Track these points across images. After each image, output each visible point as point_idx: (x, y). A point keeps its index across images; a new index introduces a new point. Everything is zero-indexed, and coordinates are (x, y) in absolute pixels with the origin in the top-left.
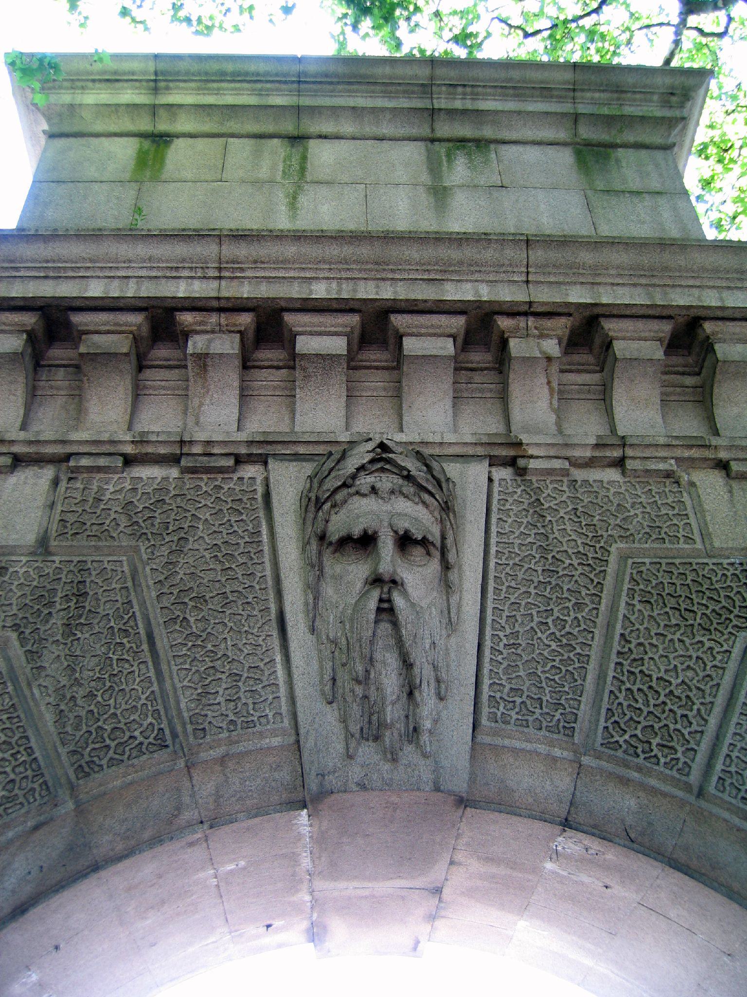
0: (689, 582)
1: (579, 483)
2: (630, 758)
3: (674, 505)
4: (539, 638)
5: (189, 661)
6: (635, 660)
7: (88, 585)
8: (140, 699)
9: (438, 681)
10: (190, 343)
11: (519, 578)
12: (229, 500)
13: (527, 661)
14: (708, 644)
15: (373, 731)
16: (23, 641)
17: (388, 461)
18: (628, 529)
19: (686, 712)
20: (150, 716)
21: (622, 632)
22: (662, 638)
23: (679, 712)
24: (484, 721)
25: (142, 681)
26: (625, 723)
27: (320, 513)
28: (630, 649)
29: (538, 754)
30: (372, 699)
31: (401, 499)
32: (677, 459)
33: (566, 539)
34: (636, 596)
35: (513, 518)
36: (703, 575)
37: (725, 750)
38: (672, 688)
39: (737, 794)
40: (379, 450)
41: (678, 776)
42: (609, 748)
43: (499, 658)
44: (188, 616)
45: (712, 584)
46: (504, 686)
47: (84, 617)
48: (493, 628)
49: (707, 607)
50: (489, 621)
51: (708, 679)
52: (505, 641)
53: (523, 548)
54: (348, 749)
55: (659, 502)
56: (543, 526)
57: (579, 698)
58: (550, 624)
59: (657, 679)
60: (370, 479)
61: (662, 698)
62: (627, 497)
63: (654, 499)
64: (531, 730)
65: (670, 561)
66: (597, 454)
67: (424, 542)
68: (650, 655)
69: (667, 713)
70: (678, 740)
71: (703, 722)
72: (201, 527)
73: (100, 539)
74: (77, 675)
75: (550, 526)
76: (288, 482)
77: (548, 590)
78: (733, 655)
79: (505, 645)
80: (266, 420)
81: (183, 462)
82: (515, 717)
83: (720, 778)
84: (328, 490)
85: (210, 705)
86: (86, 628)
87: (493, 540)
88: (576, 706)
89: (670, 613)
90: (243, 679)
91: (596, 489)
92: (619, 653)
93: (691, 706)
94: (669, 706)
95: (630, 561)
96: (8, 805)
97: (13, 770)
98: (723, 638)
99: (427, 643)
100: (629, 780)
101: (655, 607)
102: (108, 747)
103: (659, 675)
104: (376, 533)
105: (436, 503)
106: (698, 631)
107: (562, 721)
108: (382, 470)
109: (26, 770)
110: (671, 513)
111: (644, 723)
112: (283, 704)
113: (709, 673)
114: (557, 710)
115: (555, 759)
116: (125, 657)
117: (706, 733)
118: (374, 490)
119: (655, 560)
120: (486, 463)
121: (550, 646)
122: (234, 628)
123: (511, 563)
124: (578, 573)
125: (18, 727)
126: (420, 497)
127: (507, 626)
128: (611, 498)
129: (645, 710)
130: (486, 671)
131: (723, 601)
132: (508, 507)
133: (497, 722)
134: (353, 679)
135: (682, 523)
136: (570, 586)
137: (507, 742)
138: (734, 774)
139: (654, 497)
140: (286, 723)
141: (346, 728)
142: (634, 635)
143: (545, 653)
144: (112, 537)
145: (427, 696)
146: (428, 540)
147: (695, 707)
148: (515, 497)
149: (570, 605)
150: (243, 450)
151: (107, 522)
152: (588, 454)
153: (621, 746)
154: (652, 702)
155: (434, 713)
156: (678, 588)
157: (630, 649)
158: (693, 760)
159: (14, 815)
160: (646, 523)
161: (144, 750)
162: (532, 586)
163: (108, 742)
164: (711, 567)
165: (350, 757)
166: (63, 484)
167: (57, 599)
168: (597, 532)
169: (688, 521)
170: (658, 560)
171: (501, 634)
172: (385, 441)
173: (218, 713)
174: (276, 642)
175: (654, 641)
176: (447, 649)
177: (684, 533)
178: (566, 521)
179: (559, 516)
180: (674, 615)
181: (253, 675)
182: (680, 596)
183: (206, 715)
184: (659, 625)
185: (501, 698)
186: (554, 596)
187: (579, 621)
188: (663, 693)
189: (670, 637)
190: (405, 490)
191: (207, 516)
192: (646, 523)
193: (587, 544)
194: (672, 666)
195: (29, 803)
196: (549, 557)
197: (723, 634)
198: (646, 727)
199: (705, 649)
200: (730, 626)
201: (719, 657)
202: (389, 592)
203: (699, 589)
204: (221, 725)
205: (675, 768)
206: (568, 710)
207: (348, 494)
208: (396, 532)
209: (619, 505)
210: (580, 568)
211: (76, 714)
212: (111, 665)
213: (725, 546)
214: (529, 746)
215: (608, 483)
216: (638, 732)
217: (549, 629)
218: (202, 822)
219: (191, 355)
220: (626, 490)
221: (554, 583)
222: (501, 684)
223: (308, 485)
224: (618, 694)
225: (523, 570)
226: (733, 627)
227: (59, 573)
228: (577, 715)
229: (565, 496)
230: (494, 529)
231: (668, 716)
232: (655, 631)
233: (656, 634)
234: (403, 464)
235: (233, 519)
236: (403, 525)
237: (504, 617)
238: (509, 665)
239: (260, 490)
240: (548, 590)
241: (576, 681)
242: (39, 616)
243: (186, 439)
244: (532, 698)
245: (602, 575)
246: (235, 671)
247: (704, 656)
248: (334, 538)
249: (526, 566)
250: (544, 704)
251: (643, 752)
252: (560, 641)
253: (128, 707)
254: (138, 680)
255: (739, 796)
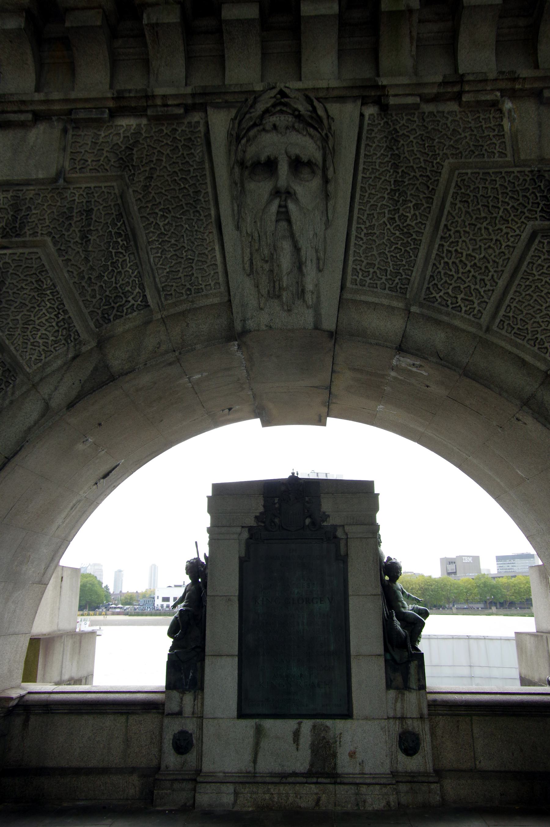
0: (497, 186)
1: (427, 114)
2: (442, 308)
3: (495, 128)
4: (388, 229)
5: (160, 251)
6: (452, 242)
7: (93, 203)
8: (131, 277)
9: (318, 259)
10: (145, 16)
11: (378, 187)
12: (182, 139)
13: (379, 244)
14: (505, 231)
15: (275, 293)
16: (55, 243)
17: (286, 105)
18: (458, 149)
19: (483, 277)
20: (137, 287)
21: (446, 223)
22: (473, 227)
23: (479, 277)
24: (348, 284)
25: (132, 265)
26: (441, 285)
27: (240, 147)
28: (450, 235)
29: (382, 305)
30: (275, 272)
31: (294, 133)
32: (501, 90)
33: (412, 158)
34: (458, 197)
35: (377, 143)
36: (509, 181)
37: (507, 302)
38: (476, 261)
39: (511, 331)
40: (279, 96)
41: (473, 319)
42: (429, 301)
43: (361, 243)
44: (158, 222)
45: (514, 187)
46: (363, 262)
47: (92, 225)
48: (358, 223)
49: (508, 204)
50: (355, 218)
51: (502, 254)
52: (365, 231)
53: (382, 165)
54: (260, 304)
55: (484, 126)
56: (397, 149)
57: (412, 269)
58: (397, 219)
59: (467, 255)
60: (274, 119)
61: (468, 268)
62: (461, 124)
63: (480, 124)
64: (379, 290)
65: (486, 171)
66: (441, 90)
67: (310, 164)
68: (463, 238)
69: (470, 278)
70: (476, 295)
71: (495, 284)
72: (164, 159)
73: (98, 171)
74: (91, 263)
75: (402, 148)
76: (220, 123)
77: (397, 195)
78: (522, 237)
79: (365, 234)
80: (204, 78)
81: (149, 112)
82: (368, 281)
83: (501, 320)
84: (244, 129)
85: (174, 279)
86: (94, 233)
87: (361, 160)
88: (410, 274)
89: (481, 209)
90: (195, 261)
91: (438, 118)
92: (442, 238)
93: (488, 273)
94: (473, 273)
95: (457, 172)
96: (55, 346)
97: (57, 325)
98: (517, 226)
99: (311, 233)
100: (440, 321)
101: (471, 205)
102: (113, 307)
103: (468, 253)
104: (276, 158)
105: (318, 135)
106: (499, 221)
107: (400, 284)
108: (282, 112)
109: (65, 324)
110: (491, 134)
111: (454, 285)
112: (220, 277)
113: (504, 250)
114: (396, 277)
115: (393, 308)
116: (120, 250)
117: (495, 292)
118: (275, 127)
119: (475, 171)
120: (359, 103)
121: (395, 234)
122: (188, 228)
123: (373, 176)
124: (419, 182)
125: (57, 298)
126: (307, 131)
127: (367, 221)
128: (449, 125)
129: (456, 276)
130: (351, 252)
131: (521, 199)
132: (373, 135)
133: (356, 285)
134: (262, 260)
135: (499, 142)
136: (412, 192)
137: (363, 298)
138: (511, 318)
139: (481, 122)
140: (223, 288)
141: (259, 292)
142: (454, 225)
143: (392, 239)
144: (107, 170)
145: (310, 270)
146: (312, 162)
147: (490, 274)
148: (379, 127)
149: (411, 205)
150: (190, 101)
151: (102, 159)
152: (435, 91)
153: (437, 300)
154: (461, 270)
155: (315, 280)
156: (489, 190)
157: (450, 235)
158: (485, 309)
159: (60, 351)
160: (472, 143)
161: (135, 309)
162: (386, 192)
163: (113, 304)
164: (516, 174)
165: (262, 309)
166: (70, 132)
167: (74, 214)
168: (435, 151)
169: (504, 140)
170: (478, 170)
171: (363, 227)
172: (284, 89)
173: (180, 284)
174: (215, 236)
175: (467, 229)
176: (325, 238)
177: (499, 150)
178: (414, 144)
179: (409, 140)
180: (484, 210)
181: (201, 259)
182: (490, 197)
183: (172, 286)
184: (472, 217)
185: (360, 269)
186: (401, 200)
187: (417, 216)
188: (469, 265)
189: (479, 226)
190: (296, 125)
191: (168, 151)
192: (472, 143)
193: (427, 161)
194: (478, 246)
195: (68, 344)
196: (400, 171)
197: (517, 223)
198: (455, 287)
199: (503, 233)
200: (523, 217)
201: (512, 239)
202: (286, 200)
203: (505, 191)
204: (181, 291)
205: (472, 314)
206: (404, 276)
207: (258, 131)
208: (290, 157)
209: (454, 130)
210: (420, 179)
211: (92, 288)
212: (112, 256)
213: (529, 158)
214: (376, 300)
215: (448, 113)
216: (450, 291)
217: (396, 222)
218: (174, 351)
219: (146, 25)
220: (461, 118)
221: (401, 190)
222: (361, 261)
223: (231, 126)
224: (438, 266)
225: (381, 181)
226: (525, 218)
227: (73, 196)
228: (409, 280)
229: (415, 125)
230: (362, 151)
231: (471, 280)
232: (469, 222)
233: (469, 224)
234: (296, 106)
235: (185, 153)
236: (295, 151)
237: (366, 216)
238: (367, 247)
239: (320, 130)
240: (397, 195)
241: (411, 257)
242: (64, 226)
243: (150, 94)
244: (381, 269)
245: (436, 183)
246: (189, 257)
247: (501, 239)
248: (249, 164)
249: (383, 178)
250: (389, 272)
251: (452, 303)
252: (403, 230)
253: (124, 282)
254: (129, 265)
255: (513, 332)
